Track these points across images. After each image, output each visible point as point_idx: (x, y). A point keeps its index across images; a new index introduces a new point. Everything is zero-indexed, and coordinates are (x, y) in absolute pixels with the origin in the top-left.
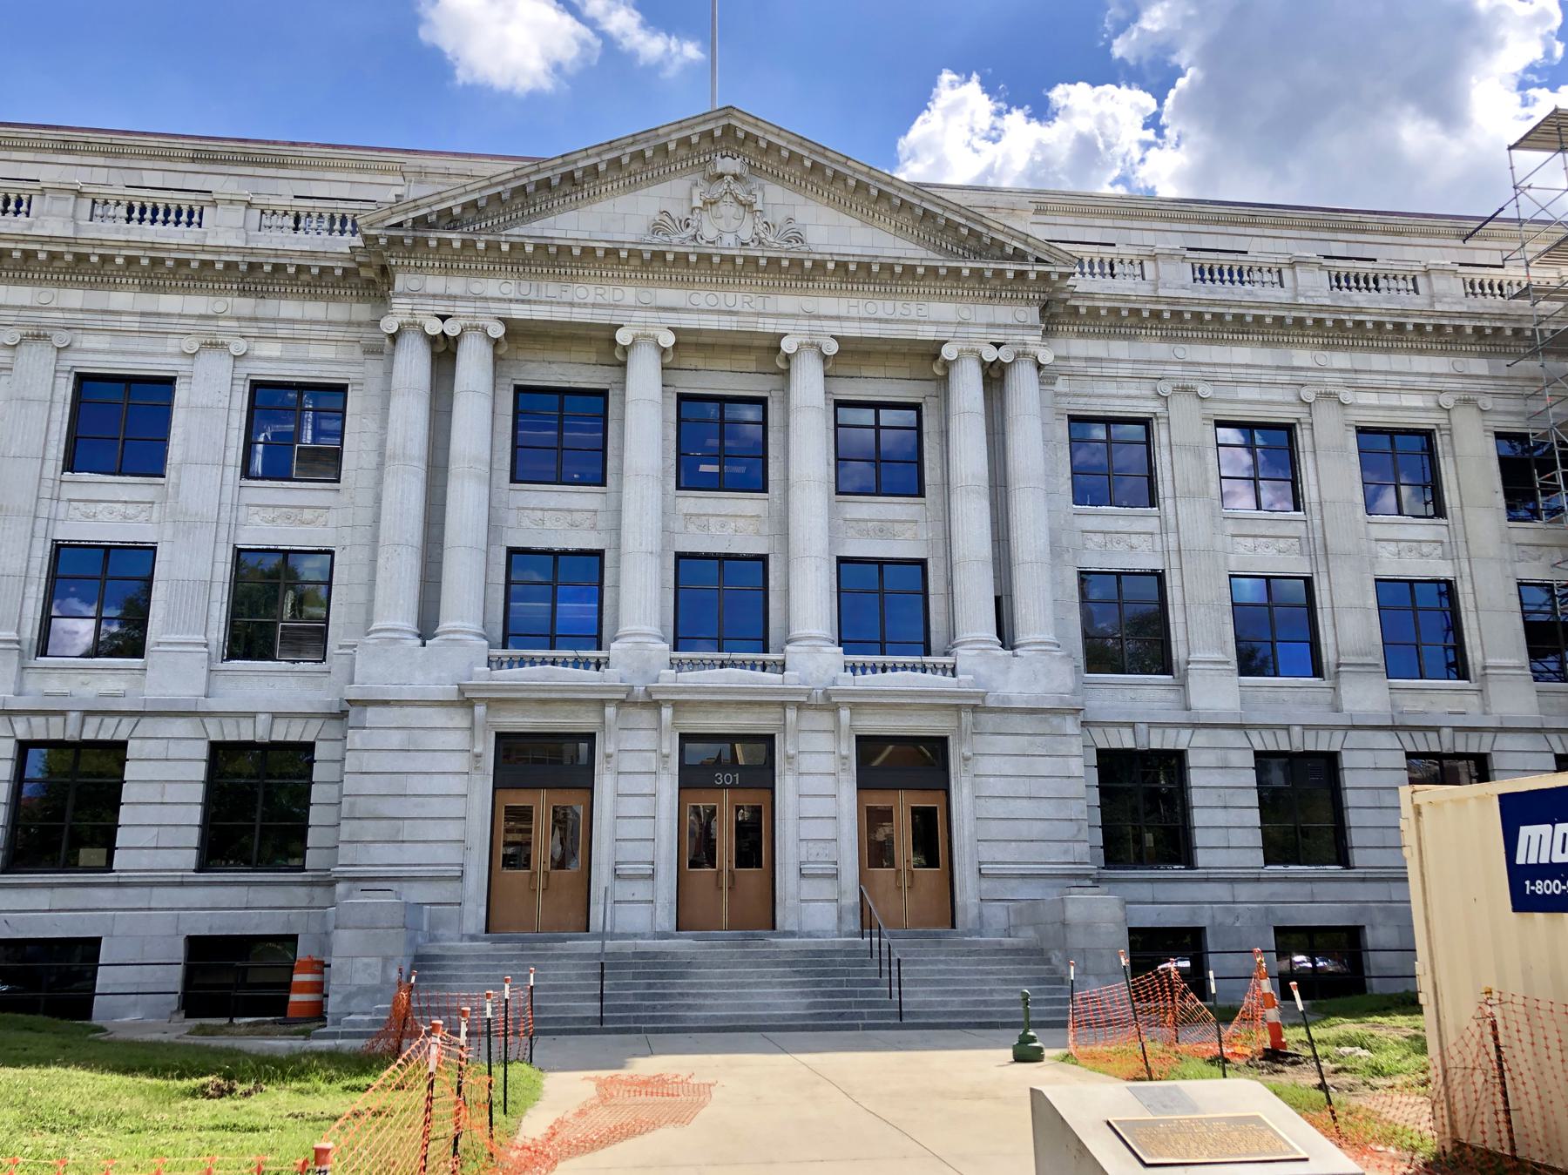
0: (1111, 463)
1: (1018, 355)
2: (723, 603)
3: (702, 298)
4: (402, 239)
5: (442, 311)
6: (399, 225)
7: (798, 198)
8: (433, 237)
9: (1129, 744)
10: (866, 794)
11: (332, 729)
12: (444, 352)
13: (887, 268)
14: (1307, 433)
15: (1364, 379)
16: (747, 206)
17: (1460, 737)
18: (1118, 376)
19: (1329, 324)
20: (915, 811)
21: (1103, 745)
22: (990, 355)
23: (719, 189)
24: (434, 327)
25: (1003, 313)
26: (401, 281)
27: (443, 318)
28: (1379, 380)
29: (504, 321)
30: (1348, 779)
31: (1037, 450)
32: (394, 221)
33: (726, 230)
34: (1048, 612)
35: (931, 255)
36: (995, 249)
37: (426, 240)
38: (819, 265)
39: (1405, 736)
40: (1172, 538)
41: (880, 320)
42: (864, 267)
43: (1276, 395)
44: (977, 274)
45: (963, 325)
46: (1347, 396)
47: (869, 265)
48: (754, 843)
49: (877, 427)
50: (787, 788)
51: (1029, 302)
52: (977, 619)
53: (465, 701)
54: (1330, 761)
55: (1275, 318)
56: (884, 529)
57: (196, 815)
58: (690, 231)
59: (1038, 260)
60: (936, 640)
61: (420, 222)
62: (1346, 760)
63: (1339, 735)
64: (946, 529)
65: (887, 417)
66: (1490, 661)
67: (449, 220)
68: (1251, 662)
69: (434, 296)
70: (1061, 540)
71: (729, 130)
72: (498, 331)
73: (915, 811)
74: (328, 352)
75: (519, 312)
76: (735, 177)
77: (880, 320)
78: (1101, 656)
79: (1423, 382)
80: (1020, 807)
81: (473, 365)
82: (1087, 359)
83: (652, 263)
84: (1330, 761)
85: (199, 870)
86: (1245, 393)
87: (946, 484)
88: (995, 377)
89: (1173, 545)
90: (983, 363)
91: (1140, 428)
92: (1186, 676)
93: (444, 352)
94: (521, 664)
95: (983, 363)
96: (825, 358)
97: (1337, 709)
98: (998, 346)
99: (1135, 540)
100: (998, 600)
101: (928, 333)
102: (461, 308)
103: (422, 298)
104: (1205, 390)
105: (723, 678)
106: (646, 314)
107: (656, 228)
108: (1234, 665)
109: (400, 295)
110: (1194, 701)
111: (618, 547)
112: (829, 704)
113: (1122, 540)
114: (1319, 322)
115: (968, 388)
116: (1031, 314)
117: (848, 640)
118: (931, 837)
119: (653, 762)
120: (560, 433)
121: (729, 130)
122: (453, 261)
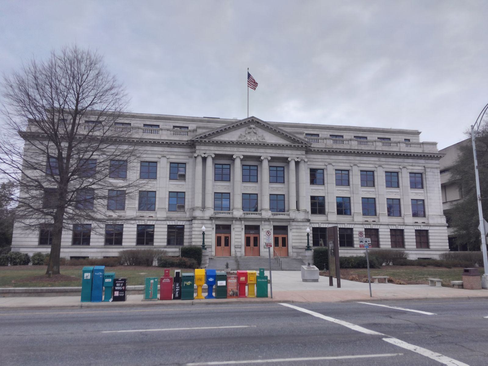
0: (316, 177)
1: (301, 160)
2: (394, 208)
3: (247, 150)
4: (198, 141)
5: (297, 157)
6: (197, 138)
7: (264, 131)
8: (203, 140)
9: (318, 226)
10: (246, 235)
11: (188, 223)
12: (204, 159)
13: (279, 145)
14: (401, 174)
15: (362, 162)
16: (255, 133)
17: (374, 226)
18: (318, 161)
19: (327, 151)
20: (282, 238)
21: (313, 227)
22: (296, 160)
23: (250, 131)
24: (203, 155)
25: (299, 152)
26: (197, 147)
27: (205, 154)
28: (364, 162)
29: (243, 155)
30: (405, 234)
31: (305, 176)
32: (197, 137)
33: (253, 139)
34: (306, 205)
35: (290, 143)
36: (298, 142)
37: (202, 141)
38: (268, 145)
39: (364, 225)
40: (327, 191)
41: (278, 154)
42: (275, 145)
43: (346, 165)
44: (298, 146)
45: (292, 155)
46: (359, 165)
47: (234, 142)
48: (227, 242)
49: (342, 174)
50: (233, 233)
51: (303, 150)
52: (293, 206)
53: (211, 219)
54: (402, 231)
55: (321, 150)
56: (277, 189)
57: (135, 237)
58: (245, 138)
59: (305, 144)
60: (286, 209)
61: (201, 137)
62: (380, 230)
63: (353, 225)
64: (286, 189)
65: (343, 172)
66: (430, 214)
67: (205, 137)
68: (415, 215)
69: (203, 150)
70: (308, 191)
71: (253, 120)
72: (213, 156)
73: (282, 238)
74: (183, 157)
75: (217, 152)
76: (254, 128)
77: (278, 154)
78: (314, 211)
79: (373, 162)
80: (299, 236)
81: (209, 162)
82: (313, 158)
83: (239, 144)
84: (402, 231)
85: (104, 246)
86: (340, 164)
87: (288, 181)
88: (297, 163)
89: (327, 192)
90: (202, 157)
91: (396, 174)
92: (428, 218)
93: (204, 159)
94: (222, 213)
95: (202, 157)
96: (212, 157)
97: (353, 221)
98: (298, 158)
99: (320, 191)
100: (297, 202)
101: (286, 156)
102: (208, 152)
103: (201, 150)
104: (334, 164)
105: (395, 220)
106: (238, 153)
107: (240, 137)
108: (336, 213)
109: (197, 150)
110: (329, 219)
111: (261, 193)
112: (268, 220)
113: (318, 191)
114: (325, 151)
115: (293, 165)
116: (304, 152)
117: (243, 209)
118: (285, 242)
119: (240, 229)
120: (223, 175)
121: (253, 120)
122: (205, 144)
